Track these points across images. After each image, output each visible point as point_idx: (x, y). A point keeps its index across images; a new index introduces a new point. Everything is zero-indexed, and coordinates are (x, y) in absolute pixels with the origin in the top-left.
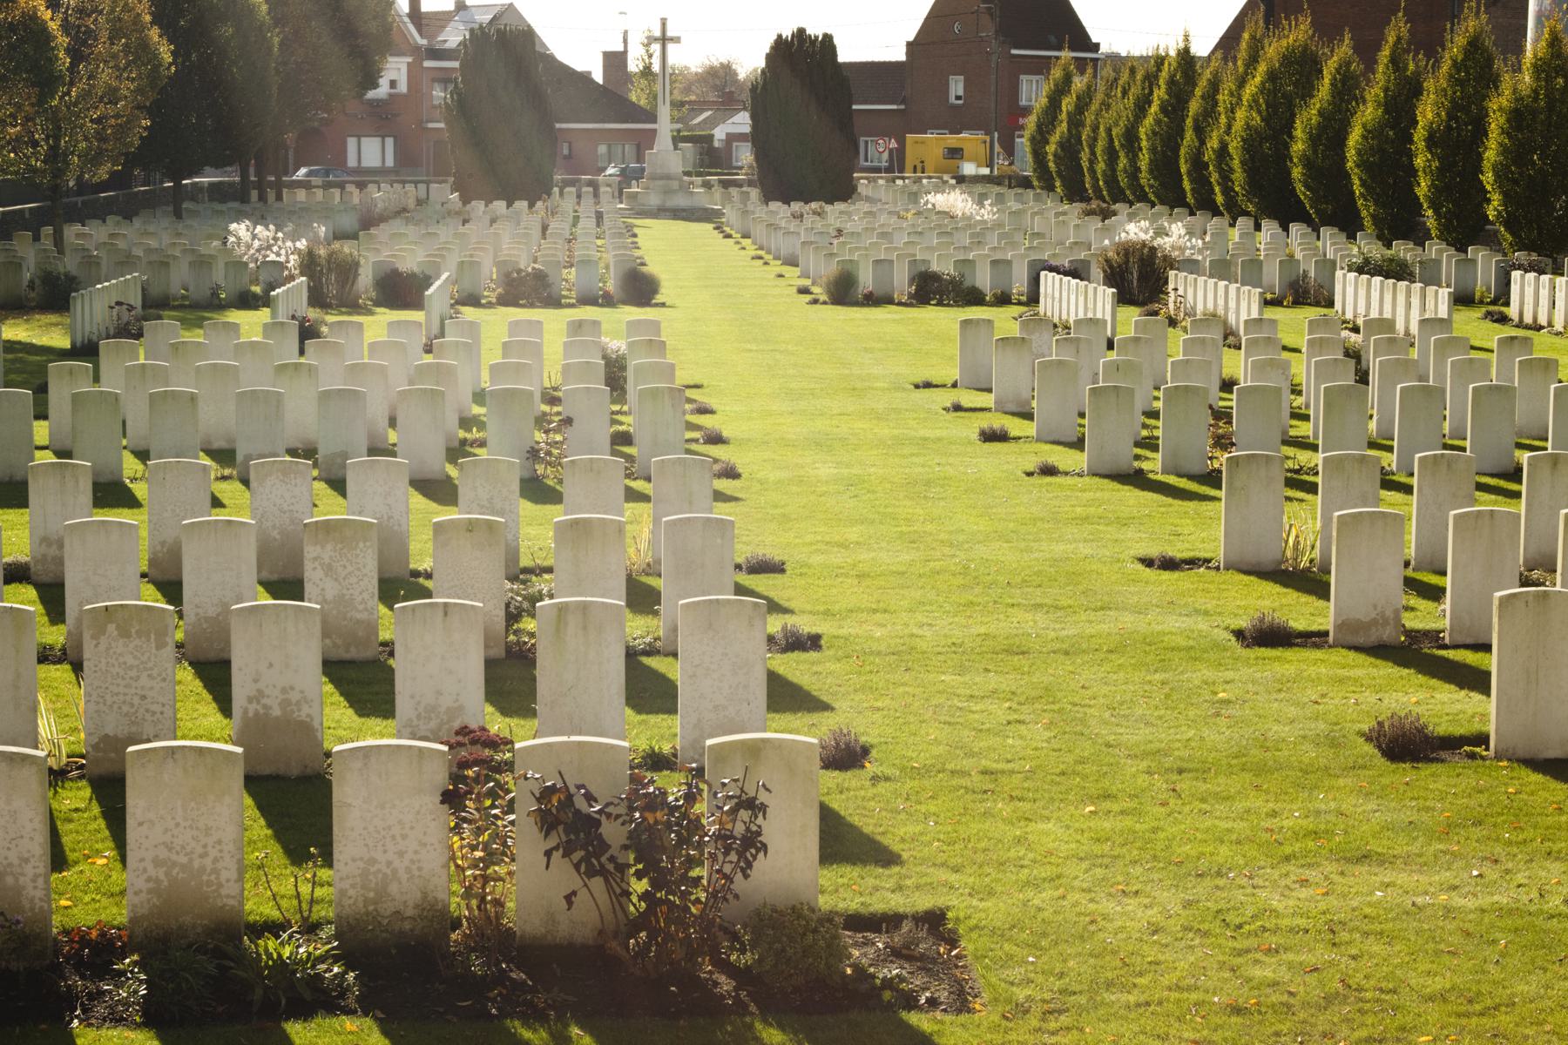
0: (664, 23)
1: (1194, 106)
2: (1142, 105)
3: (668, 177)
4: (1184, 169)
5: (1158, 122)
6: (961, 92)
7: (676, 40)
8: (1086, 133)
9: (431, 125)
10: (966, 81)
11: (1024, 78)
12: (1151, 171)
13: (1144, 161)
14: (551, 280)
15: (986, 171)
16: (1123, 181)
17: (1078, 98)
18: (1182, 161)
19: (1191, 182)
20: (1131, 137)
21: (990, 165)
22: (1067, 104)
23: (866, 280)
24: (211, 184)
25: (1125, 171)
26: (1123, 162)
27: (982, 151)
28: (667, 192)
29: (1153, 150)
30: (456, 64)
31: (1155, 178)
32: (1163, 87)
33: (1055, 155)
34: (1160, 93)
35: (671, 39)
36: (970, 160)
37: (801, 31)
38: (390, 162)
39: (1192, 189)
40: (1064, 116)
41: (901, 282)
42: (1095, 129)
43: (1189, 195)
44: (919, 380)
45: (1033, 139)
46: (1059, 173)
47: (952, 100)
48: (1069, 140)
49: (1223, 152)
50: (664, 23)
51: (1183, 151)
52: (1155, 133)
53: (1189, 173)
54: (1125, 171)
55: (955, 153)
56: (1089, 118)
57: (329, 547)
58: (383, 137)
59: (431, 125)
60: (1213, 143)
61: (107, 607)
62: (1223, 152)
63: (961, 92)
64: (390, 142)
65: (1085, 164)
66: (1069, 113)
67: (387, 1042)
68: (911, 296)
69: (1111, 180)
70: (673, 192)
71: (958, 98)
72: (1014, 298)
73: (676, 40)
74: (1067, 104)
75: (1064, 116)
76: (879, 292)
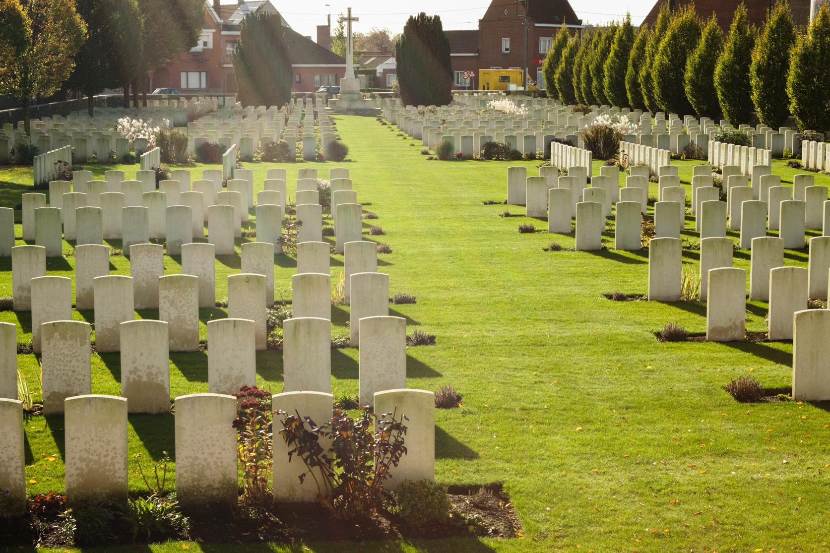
0: (349, 10)
1: (633, 53)
2: (605, 53)
3: (352, 93)
4: (627, 87)
5: (613, 62)
6: (508, 47)
7: (356, 19)
8: (575, 68)
9: (225, 66)
12: (610, 88)
13: (606, 83)
15: (522, 88)
16: (595, 93)
17: (571, 49)
18: (626, 82)
19: (631, 94)
20: (599, 70)
21: (524, 85)
22: (565, 52)
23: (458, 147)
24: (108, 98)
27: (520, 78)
28: (352, 101)
29: (611, 77)
30: (239, 33)
31: (612, 92)
32: (616, 43)
33: (559, 80)
34: (614, 47)
36: (513, 83)
37: (423, 14)
38: (204, 85)
39: (632, 98)
41: (477, 148)
42: (580, 65)
44: (486, 200)
45: (547, 72)
46: (561, 89)
47: (504, 51)
48: (566, 72)
49: (648, 77)
50: (349, 10)
51: (627, 77)
53: (630, 89)
54: (596, 88)
55: (505, 79)
56: (577, 60)
58: (200, 72)
59: (225, 66)
62: (648, 77)
63: (508, 47)
64: (204, 75)
65: (575, 85)
68: (482, 155)
69: (589, 93)
71: (507, 49)
72: (537, 156)
73: (356, 19)
74: (565, 52)
76: (465, 153)
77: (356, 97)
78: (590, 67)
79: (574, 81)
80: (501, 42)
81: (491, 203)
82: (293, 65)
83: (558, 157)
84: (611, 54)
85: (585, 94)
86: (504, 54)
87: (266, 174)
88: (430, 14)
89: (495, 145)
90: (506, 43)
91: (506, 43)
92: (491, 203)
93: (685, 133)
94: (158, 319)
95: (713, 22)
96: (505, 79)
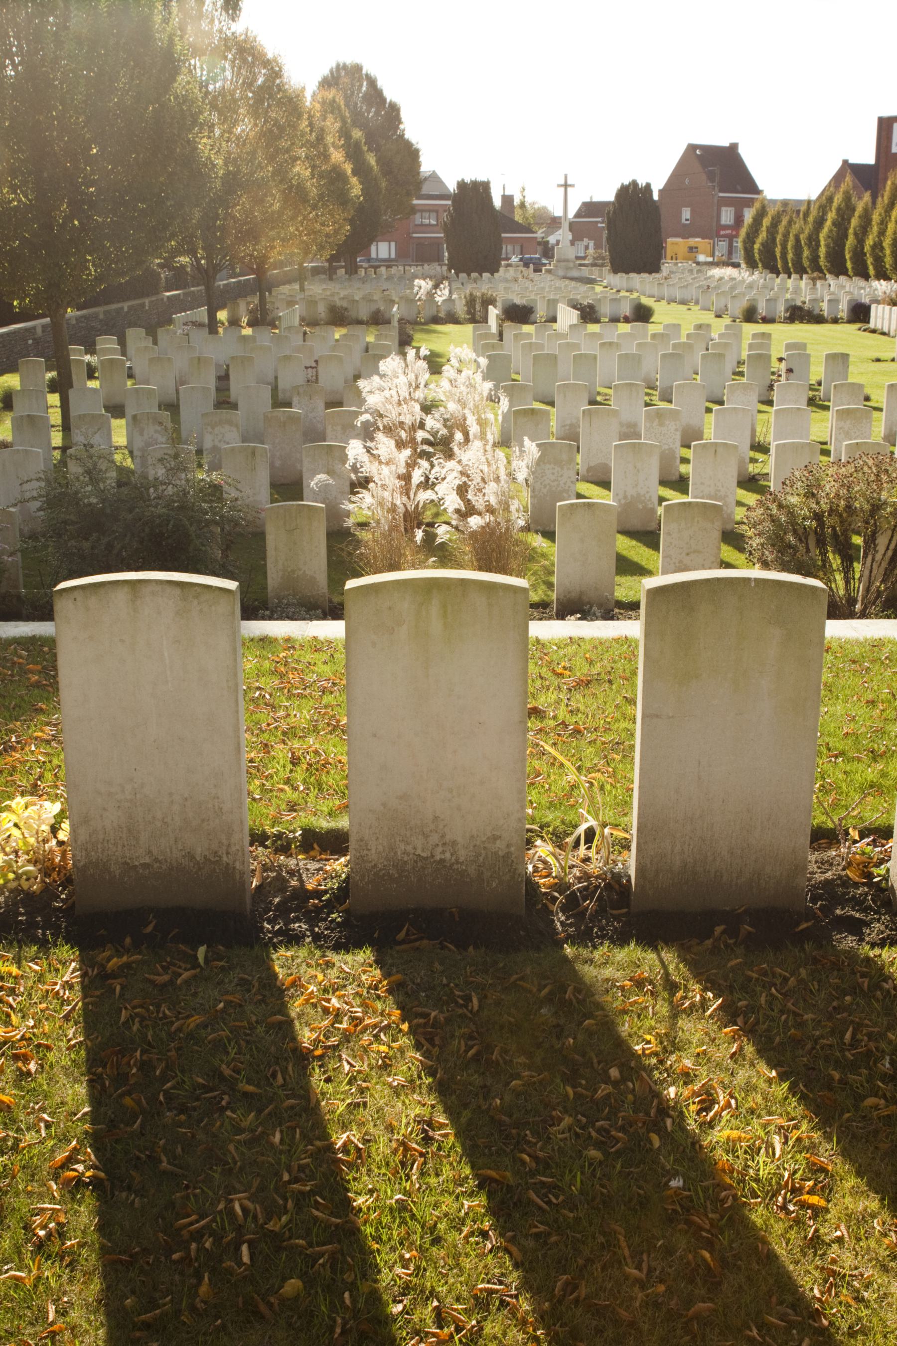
1: (854, 222)
2: (819, 223)
3: (567, 261)
4: (847, 256)
5: (831, 231)
6: (688, 217)
7: (572, 186)
8: (779, 238)
9: (415, 235)
10: (692, 211)
11: (724, 209)
12: (826, 257)
13: (822, 251)
14: (597, 309)
16: (806, 263)
17: (773, 218)
18: (847, 252)
19: (853, 263)
21: (713, 255)
22: (766, 222)
23: (762, 310)
24: (313, 267)
25: (808, 258)
26: (806, 253)
27: (708, 248)
28: (568, 268)
29: (827, 246)
30: (449, 202)
31: (828, 262)
32: (834, 211)
33: (759, 250)
34: (831, 216)
35: (570, 186)
36: (702, 253)
38: (393, 256)
39: (853, 268)
40: (764, 228)
41: (781, 310)
42: (786, 236)
43: (850, 270)
44: (874, 358)
45: (744, 242)
46: (760, 260)
47: (683, 221)
48: (766, 242)
49: (878, 246)
52: (829, 237)
53: (851, 258)
54: (808, 258)
55: (692, 249)
56: (781, 229)
57: (848, 422)
58: (390, 242)
59: (415, 235)
60: (870, 242)
61: (857, 443)
62: (878, 246)
63: (688, 217)
64: (393, 244)
65: (778, 255)
66: (767, 227)
67: (4, 636)
68: (785, 318)
70: (571, 269)
71: (687, 220)
72: (777, 320)
73: (572, 186)
74: (766, 222)
75: (764, 228)
76: (769, 317)
77: (571, 265)
78: (802, 236)
79: (778, 251)
80: (681, 213)
81: (878, 360)
82: (503, 235)
83: (883, 319)
84: (828, 223)
85: (793, 264)
86: (685, 225)
87: (723, 328)
88: (642, 182)
89: (800, 309)
90: (686, 214)
91: (686, 214)
92: (878, 360)
93: (597, 321)
94: (302, 500)
95: (867, 197)
96: (692, 249)
